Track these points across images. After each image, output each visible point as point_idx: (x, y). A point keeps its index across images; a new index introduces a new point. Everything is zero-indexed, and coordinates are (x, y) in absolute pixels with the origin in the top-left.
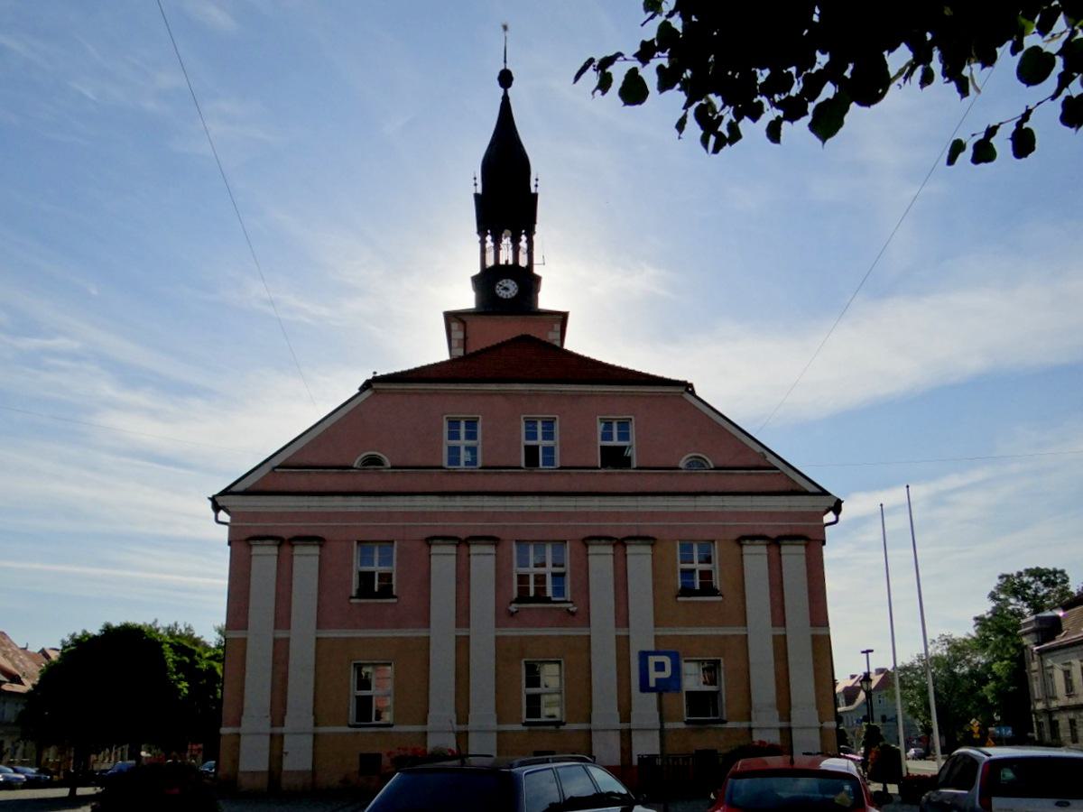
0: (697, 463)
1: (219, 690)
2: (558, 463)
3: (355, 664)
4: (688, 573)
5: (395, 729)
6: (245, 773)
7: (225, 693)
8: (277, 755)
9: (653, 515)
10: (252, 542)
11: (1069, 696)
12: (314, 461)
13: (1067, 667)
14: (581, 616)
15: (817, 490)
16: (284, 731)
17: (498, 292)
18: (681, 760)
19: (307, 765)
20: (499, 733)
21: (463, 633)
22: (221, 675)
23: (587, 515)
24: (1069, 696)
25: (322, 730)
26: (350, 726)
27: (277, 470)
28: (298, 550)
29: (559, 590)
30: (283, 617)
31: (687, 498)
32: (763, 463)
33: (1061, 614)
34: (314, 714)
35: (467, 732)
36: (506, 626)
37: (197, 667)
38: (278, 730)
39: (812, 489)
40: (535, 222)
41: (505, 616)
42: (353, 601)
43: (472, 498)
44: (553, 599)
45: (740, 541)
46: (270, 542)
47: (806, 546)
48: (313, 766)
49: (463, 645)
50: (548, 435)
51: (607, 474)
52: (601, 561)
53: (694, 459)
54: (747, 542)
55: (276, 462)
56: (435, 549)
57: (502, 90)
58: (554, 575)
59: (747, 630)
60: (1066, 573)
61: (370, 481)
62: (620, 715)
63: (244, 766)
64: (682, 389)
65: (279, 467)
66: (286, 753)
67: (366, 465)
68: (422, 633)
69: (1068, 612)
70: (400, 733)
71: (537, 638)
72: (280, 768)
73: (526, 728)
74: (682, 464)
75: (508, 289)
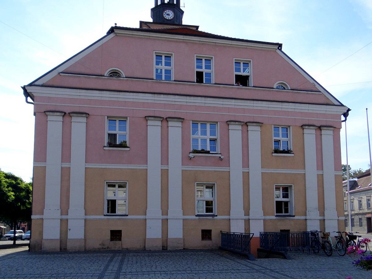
0: (283, 87)
1: (31, 198)
3: (107, 183)
4: (277, 142)
7: (35, 198)
9: (261, 111)
10: (47, 113)
11: (360, 210)
12: (83, 70)
13: (359, 199)
14: (223, 160)
15: (339, 104)
16: (68, 218)
17: (164, 16)
21: (165, 167)
22: (31, 190)
23: (229, 110)
24: (360, 210)
25: (88, 217)
26: (104, 215)
27: (60, 74)
28: (74, 119)
29: (214, 148)
30: (66, 156)
31: (276, 103)
32: (314, 89)
33: (356, 179)
34: (85, 209)
36: (187, 165)
37: (19, 186)
38: (64, 217)
39: (337, 103)
41: (187, 159)
42: (105, 148)
44: (211, 152)
45: (302, 127)
46: (58, 114)
47: (333, 130)
48: (85, 235)
50: (208, 67)
51: (239, 88)
52: (235, 133)
53: (281, 85)
54: (307, 127)
55: (61, 69)
56: (149, 123)
58: (211, 140)
59: (305, 171)
60: (350, 166)
61: (114, 83)
62: (245, 212)
63: (46, 235)
64: (276, 47)
65: (61, 73)
66: (70, 230)
67: (111, 76)
68: (143, 167)
69: (359, 179)
70: (132, 219)
71: (203, 172)
74: (275, 86)
75: (169, 15)
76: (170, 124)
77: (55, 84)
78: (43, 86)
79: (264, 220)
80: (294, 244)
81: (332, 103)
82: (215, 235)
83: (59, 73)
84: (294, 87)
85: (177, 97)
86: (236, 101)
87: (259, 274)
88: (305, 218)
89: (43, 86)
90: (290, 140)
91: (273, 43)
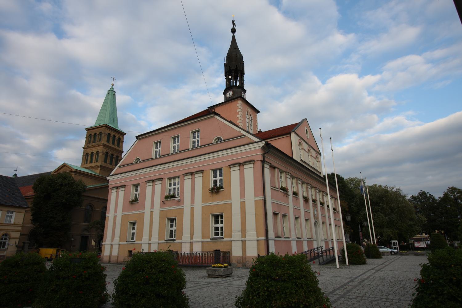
2: (179, 151)
5: (136, 242)
6: (113, 256)
18: (200, 254)
19: (117, 255)
25: (121, 243)
32: (240, 135)
35: (245, 241)
38: (243, 239)
46: (115, 188)
49: (243, 205)
57: (232, 34)
65: (119, 166)
72: (111, 255)
73: (165, 242)
80: (206, 262)
81: (253, 142)
84: (226, 138)
88: (241, 240)
89: (113, 175)
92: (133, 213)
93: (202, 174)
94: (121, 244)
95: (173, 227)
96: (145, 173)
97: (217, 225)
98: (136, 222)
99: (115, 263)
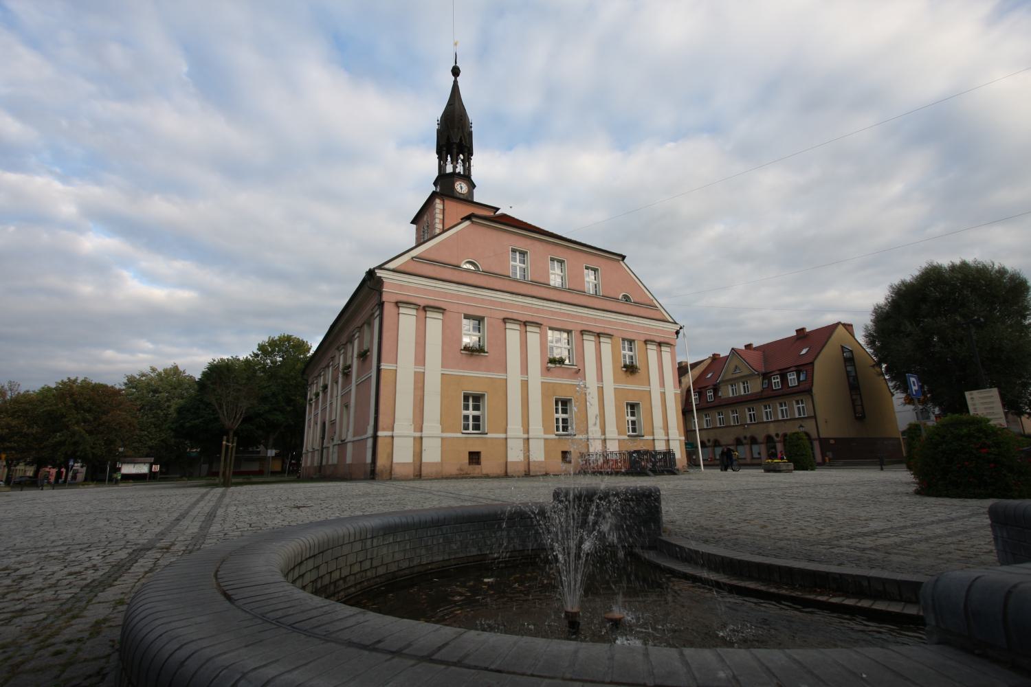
6: (510, 462)
8: (419, 453)
14: (579, 372)
20: (442, 439)
23: (649, 329)
39: (671, 320)
40: (438, 131)
43: (462, 286)
56: (402, 310)
65: (415, 257)
76: (429, 314)
77: (408, 270)
78: (394, 271)
79: (442, 439)
82: (574, 457)
83: (412, 258)
84: (637, 300)
85: (534, 299)
86: (589, 310)
87: (835, 481)
89: (394, 271)
90: (572, 348)
91: (547, 232)
92: (475, 376)
93: (441, 315)
94: (446, 438)
95: (468, 410)
96: (580, 314)
97: (466, 412)
98: (484, 395)
99: (498, 477)
